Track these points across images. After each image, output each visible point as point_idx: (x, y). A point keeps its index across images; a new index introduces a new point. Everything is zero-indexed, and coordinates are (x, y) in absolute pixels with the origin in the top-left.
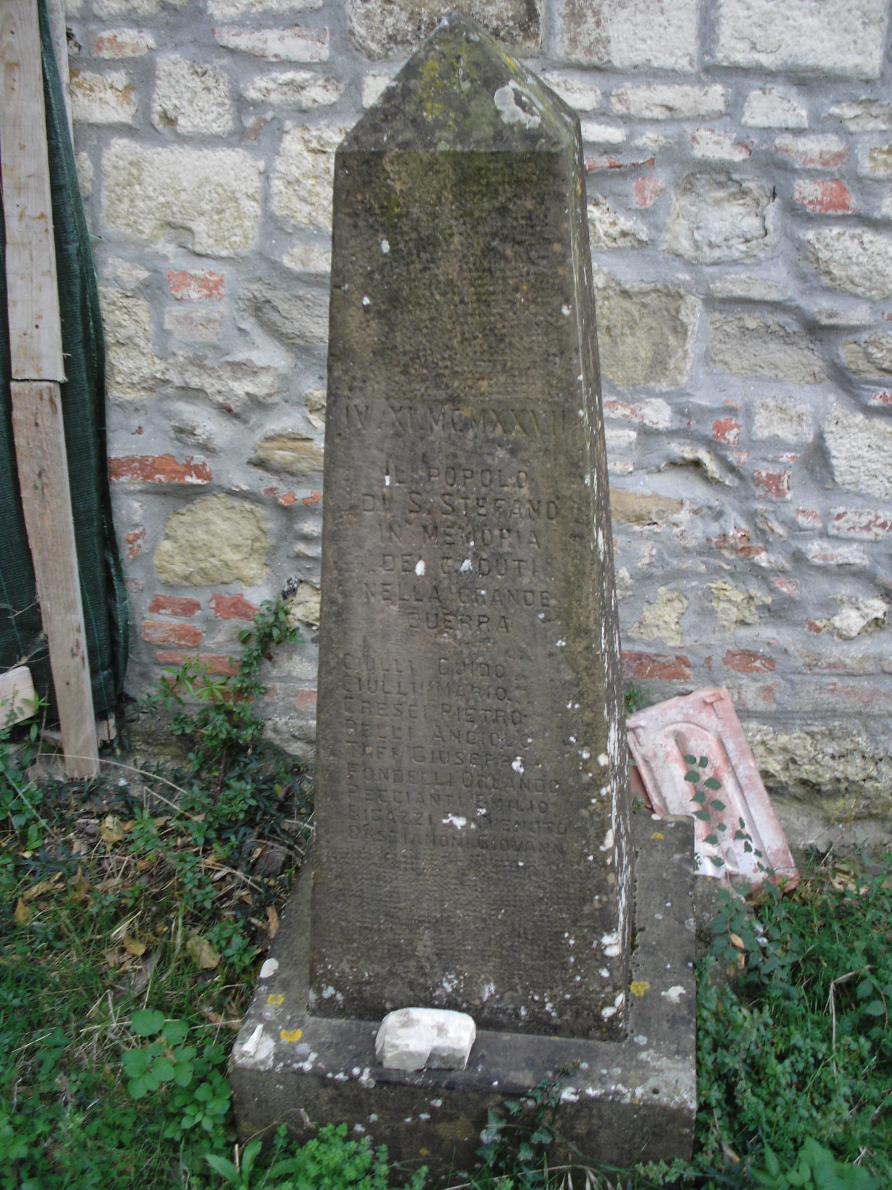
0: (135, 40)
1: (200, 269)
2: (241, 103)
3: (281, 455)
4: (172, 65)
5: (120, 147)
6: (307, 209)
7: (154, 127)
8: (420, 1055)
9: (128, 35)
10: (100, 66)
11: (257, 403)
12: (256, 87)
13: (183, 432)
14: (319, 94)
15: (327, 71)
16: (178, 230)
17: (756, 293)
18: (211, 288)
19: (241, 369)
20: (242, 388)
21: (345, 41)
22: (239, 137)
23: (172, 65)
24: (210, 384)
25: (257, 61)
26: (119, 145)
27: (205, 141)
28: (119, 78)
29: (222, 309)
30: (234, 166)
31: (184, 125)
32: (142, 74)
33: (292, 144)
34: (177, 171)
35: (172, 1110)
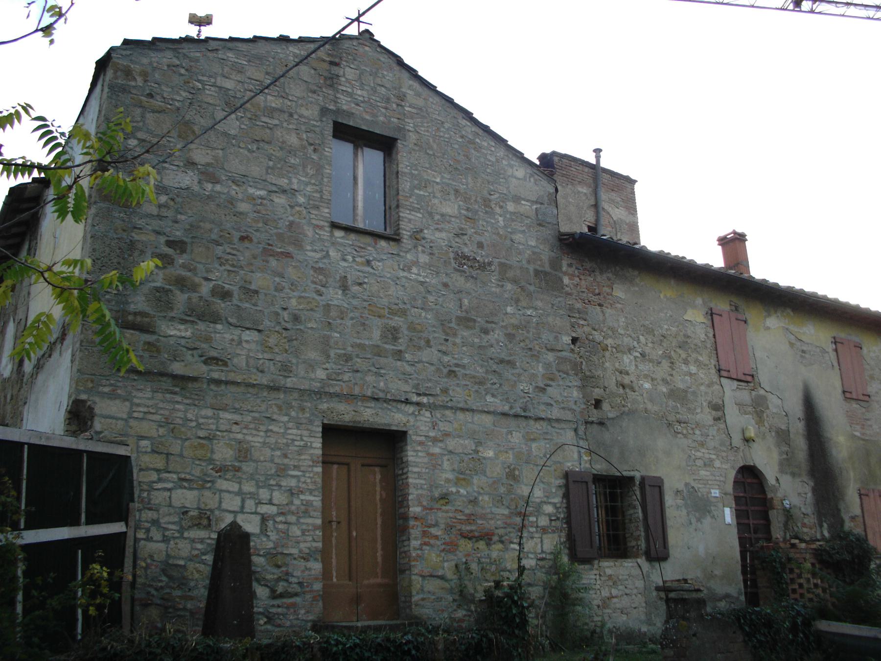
0: (147, 525)
1: (155, 563)
2: (164, 536)
3: (166, 597)
4: (153, 529)
5: (142, 542)
6: (220, 56)
7: (149, 539)
8: (634, 228)
9: (146, 524)
10: (140, 528)
11: (162, 588)
12: (167, 533)
13: (148, 593)
14: (177, 535)
15: (178, 531)
16: (151, 557)
17: (230, 509)
18: (157, 566)
19: (161, 581)
20: (160, 584)
21: (181, 527)
22: (163, 541)
23: (153, 529)
24: (154, 584)
25: (166, 529)
26: (142, 542)
27: (158, 542)
28: (144, 531)
29: (158, 570)
30: (162, 546)
31: (154, 539)
32: (148, 530)
33: (172, 542)
34: (152, 546)
35: (418, 236)
